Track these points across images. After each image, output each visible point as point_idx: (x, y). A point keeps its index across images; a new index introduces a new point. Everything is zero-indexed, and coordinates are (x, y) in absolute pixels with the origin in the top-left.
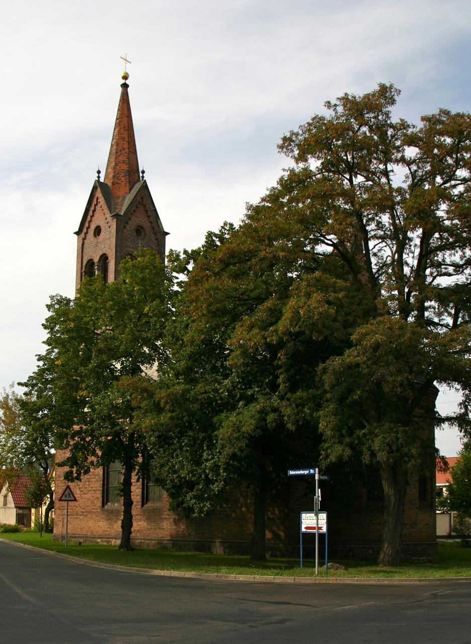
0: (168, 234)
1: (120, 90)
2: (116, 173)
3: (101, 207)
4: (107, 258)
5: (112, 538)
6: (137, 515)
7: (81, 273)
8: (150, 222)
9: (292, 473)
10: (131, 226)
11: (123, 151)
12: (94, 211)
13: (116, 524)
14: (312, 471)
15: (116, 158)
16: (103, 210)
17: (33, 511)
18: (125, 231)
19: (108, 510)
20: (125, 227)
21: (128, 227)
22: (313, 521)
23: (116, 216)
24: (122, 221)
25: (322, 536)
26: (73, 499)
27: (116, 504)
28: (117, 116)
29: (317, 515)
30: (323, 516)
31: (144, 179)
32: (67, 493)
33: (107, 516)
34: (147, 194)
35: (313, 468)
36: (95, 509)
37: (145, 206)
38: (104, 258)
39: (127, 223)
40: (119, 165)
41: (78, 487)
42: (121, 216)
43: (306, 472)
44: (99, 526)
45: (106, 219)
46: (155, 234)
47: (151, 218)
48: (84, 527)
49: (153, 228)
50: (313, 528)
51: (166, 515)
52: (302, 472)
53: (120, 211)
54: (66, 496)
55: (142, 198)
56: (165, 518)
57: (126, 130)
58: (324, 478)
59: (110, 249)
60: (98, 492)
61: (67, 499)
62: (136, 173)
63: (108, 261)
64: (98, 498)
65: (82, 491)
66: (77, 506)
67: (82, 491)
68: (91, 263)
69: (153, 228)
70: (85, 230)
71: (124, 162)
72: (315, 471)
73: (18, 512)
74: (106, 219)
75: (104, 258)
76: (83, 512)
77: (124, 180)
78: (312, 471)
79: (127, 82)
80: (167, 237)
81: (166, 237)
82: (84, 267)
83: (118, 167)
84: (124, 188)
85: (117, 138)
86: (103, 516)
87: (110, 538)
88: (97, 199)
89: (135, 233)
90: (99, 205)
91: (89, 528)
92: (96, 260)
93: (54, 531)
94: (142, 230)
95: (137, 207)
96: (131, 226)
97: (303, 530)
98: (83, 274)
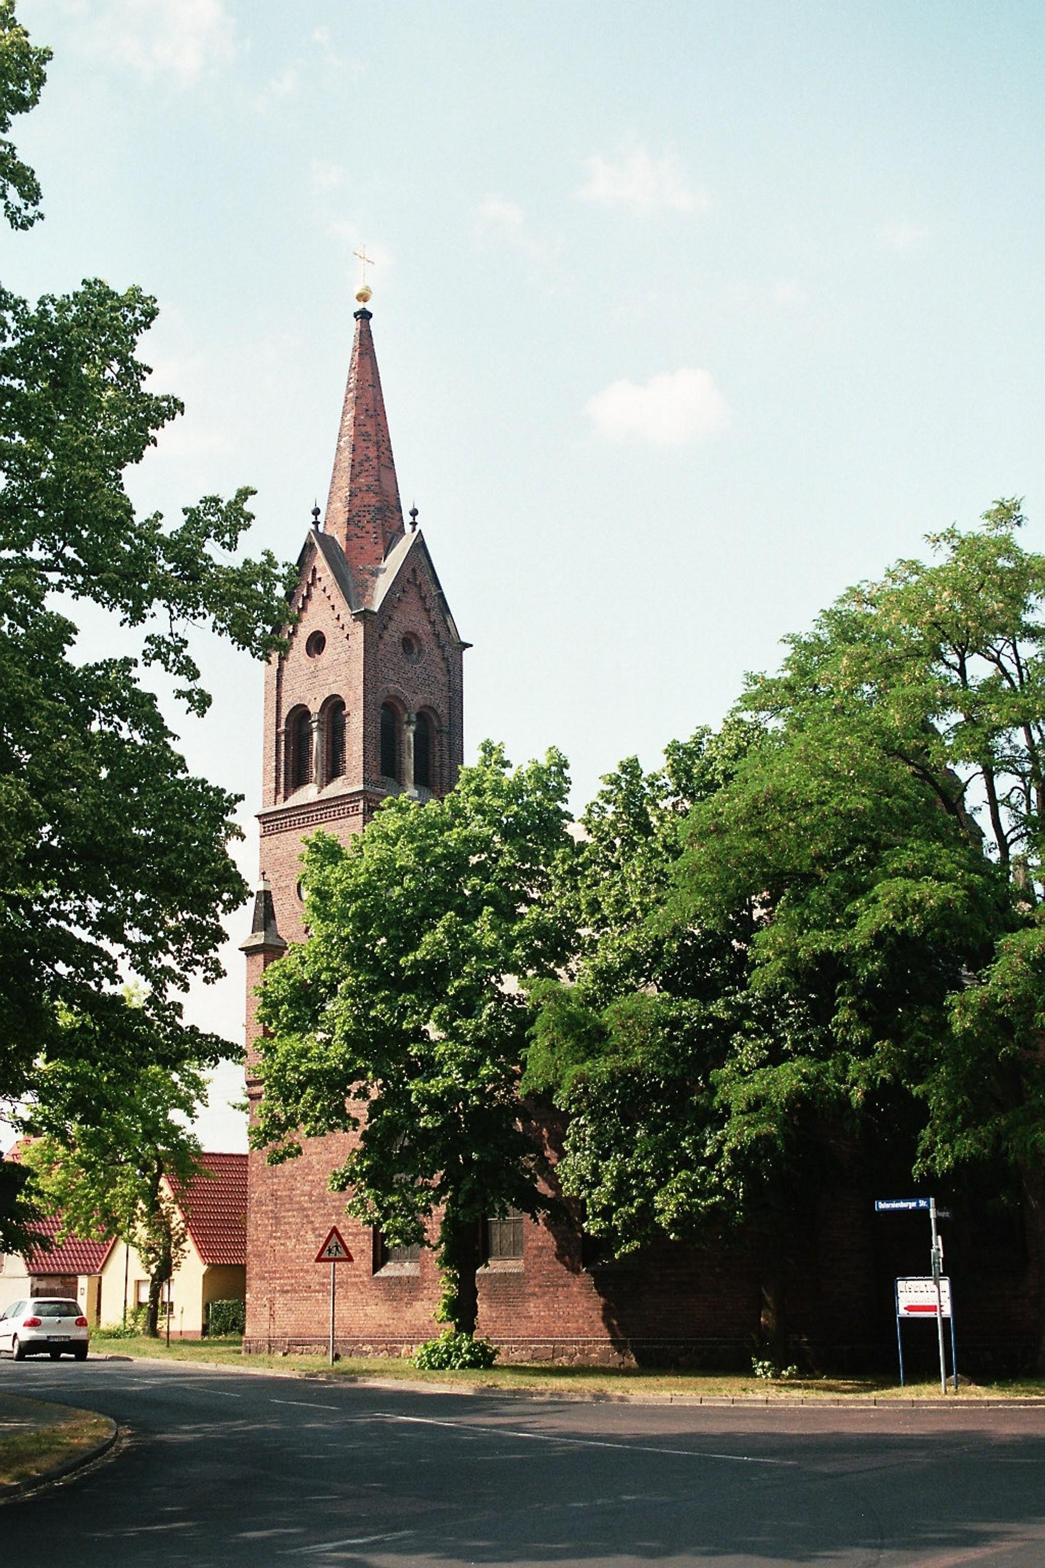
1: (354, 325)
3: (324, 590)
4: (342, 705)
5: (401, 1342)
7: (278, 735)
8: (430, 622)
9: (882, 1206)
10: (393, 634)
11: (366, 465)
14: (922, 1203)
15: (352, 480)
16: (329, 597)
17: (83, 1282)
18: (381, 646)
20: (381, 637)
21: (386, 637)
22: (922, 1296)
23: (364, 616)
25: (945, 1321)
26: (344, 1255)
28: (349, 383)
29: (937, 1284)
30: (945, 1285)
31: (418, 528)
32: (332, 1244)
33: (387, 1292)
34: (425, 562)
35: (925, 1197)
36: (355, 1276)
38: (334, 706)
39: (385, 628)
41: (310, 1226)
42: (375, 614)
43: (912, 1205)
44: (366, 1315)
45: (338, 618)
46: (442, 648)
47: (433, 613)
49: (437, 636)
50: (933, 1308)
51: (535, 1286)
52: (902, 1205)
53: (370, 602)
54: (330, 1251)
55: (414, 570)
56: (534, 1294)
57: (371, 416)
58: (945, 1214)
60: (361, 1237)
61: (332, 1256)
62: (396, 513)
63: (344, 712)
64: (363, 1251)
66: (307, 1271)
69: (437, 636)
72: (928, 1203)
73: (35, 1288)
74: (338, 618)
75: (334, 706)
76: (323, 1284)
78: (922, 1203)
79: (369, 306)
80: (466, 653)
82: (283, 722)
83: (357, 501)
84: (371, 544)
85: (352, 433)
86: (377, 1293)
87: (396, 1342)
89: (401, 649)
90: (320, 585)
92: (314, 708)
93: (247, 1330)
94: (413, 641)
95: (404, 591)
96: (393, 634)
97: (902, 1312)
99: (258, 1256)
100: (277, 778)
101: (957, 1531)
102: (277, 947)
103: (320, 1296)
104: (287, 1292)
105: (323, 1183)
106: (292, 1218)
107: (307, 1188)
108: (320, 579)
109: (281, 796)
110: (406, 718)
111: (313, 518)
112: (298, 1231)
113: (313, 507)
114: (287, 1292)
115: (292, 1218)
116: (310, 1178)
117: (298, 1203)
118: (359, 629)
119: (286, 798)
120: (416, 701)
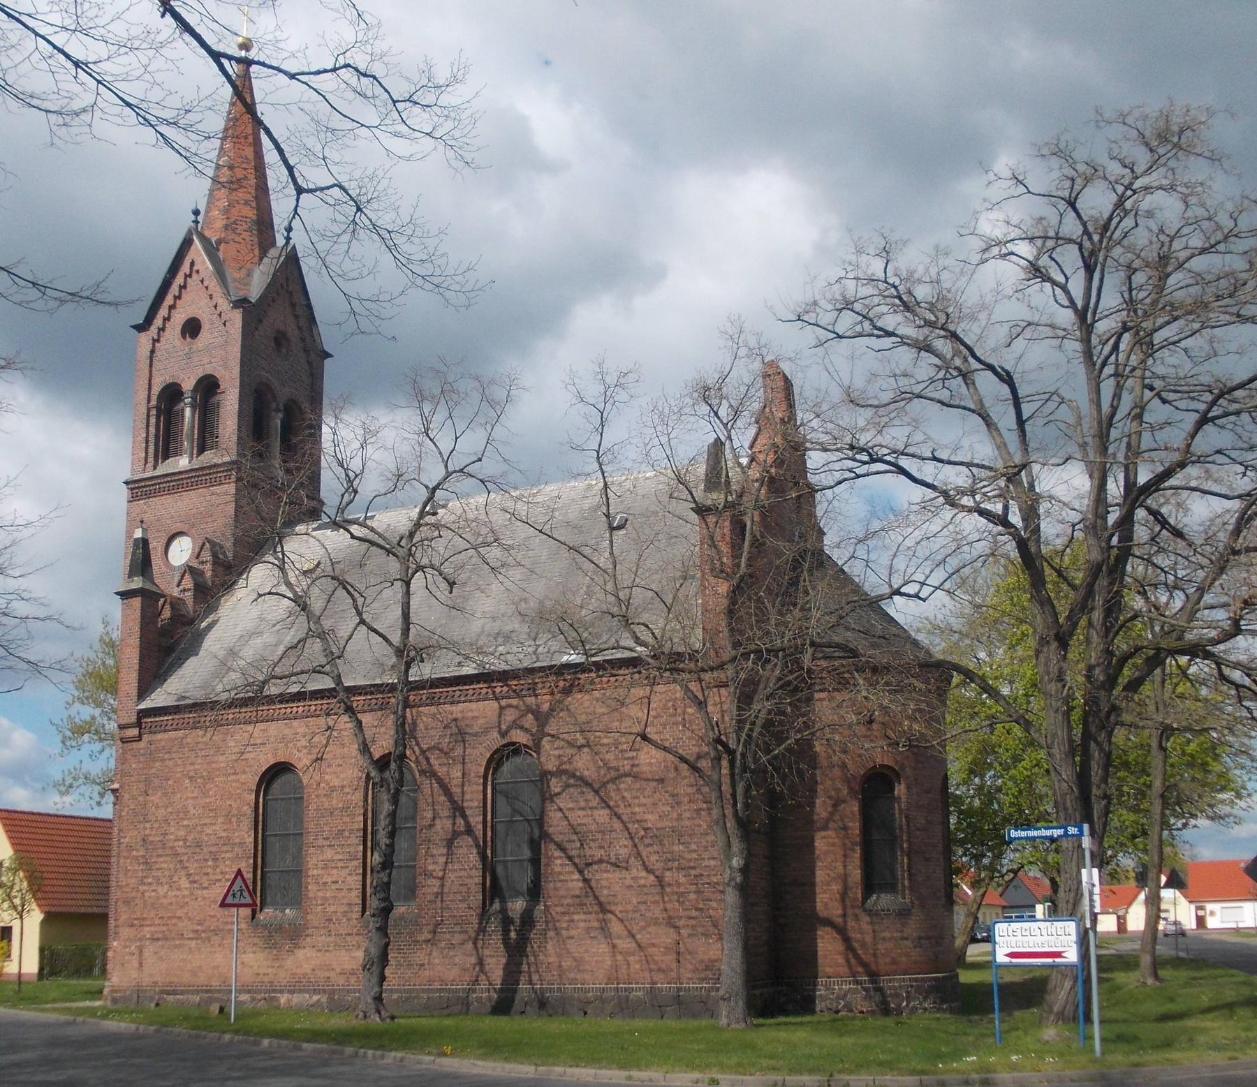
0: (328, 355)
2: (232, 220)
5: (281, 992)
6: (349, 934)
7: (149, 410)
12: (183, 287)
13: (292, 958)
19: (265, 926)
23: (242, 303)
24: (253, 312)
27: (287, 911)
31: (292, 242)
37: (291, 294)
38: (208, 386)
39: (261, 321)
40: (238, 207)
46: (306, 351)
48: (200, 967)
59: (226, 367)
61: (236, 901)
65: (195, 882)
66: (180, 918)
67: (195, 882)
68: (172, 394)
70: (158, 322)
71: (246, 203)
72: (1081, 831)
74: (216, 307)
75: (208, 386)
76: (197, 931)
77: (249, 238)
80: (327, 362)
81: (326, 361)
86: (256, 940)
87: (274, 991)
88: (192, 264)
91: (217, 967)
92: (188, 385)
98: (154, 412)
99: (127, 902)
100: (147, 448)
101: (325, 1076)
102: (155, 593)
103: (193, 943)
104: (158, 939)
105: (199, 828)
106: (166, 864)
107: (182, 833)
108: (198, 272)
109: (150, 465)
110: (274, 405)
111: (193, 217)
112: (171, 877)
113: (194, 207)
114: (158, 939)
115: (166, 864)
116: (185, 823)
117: (172, 848)
118: (237, 317)
119: (155, 468)
120: (284, 393)
